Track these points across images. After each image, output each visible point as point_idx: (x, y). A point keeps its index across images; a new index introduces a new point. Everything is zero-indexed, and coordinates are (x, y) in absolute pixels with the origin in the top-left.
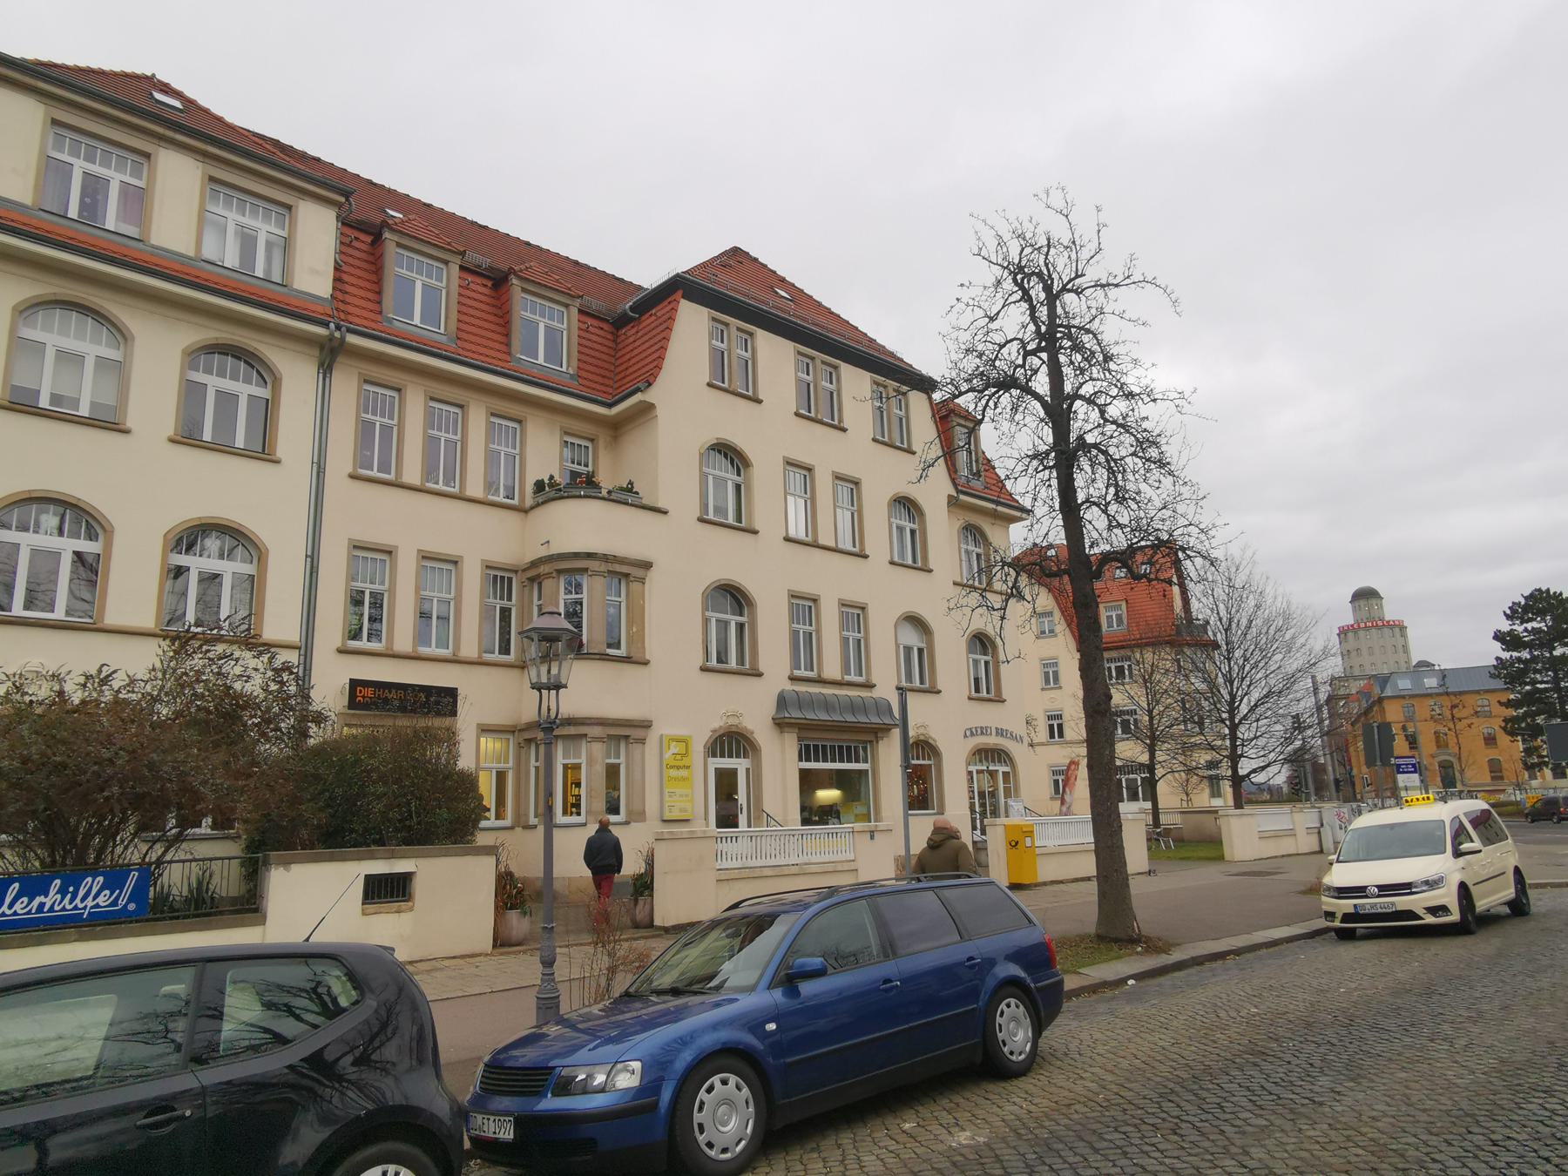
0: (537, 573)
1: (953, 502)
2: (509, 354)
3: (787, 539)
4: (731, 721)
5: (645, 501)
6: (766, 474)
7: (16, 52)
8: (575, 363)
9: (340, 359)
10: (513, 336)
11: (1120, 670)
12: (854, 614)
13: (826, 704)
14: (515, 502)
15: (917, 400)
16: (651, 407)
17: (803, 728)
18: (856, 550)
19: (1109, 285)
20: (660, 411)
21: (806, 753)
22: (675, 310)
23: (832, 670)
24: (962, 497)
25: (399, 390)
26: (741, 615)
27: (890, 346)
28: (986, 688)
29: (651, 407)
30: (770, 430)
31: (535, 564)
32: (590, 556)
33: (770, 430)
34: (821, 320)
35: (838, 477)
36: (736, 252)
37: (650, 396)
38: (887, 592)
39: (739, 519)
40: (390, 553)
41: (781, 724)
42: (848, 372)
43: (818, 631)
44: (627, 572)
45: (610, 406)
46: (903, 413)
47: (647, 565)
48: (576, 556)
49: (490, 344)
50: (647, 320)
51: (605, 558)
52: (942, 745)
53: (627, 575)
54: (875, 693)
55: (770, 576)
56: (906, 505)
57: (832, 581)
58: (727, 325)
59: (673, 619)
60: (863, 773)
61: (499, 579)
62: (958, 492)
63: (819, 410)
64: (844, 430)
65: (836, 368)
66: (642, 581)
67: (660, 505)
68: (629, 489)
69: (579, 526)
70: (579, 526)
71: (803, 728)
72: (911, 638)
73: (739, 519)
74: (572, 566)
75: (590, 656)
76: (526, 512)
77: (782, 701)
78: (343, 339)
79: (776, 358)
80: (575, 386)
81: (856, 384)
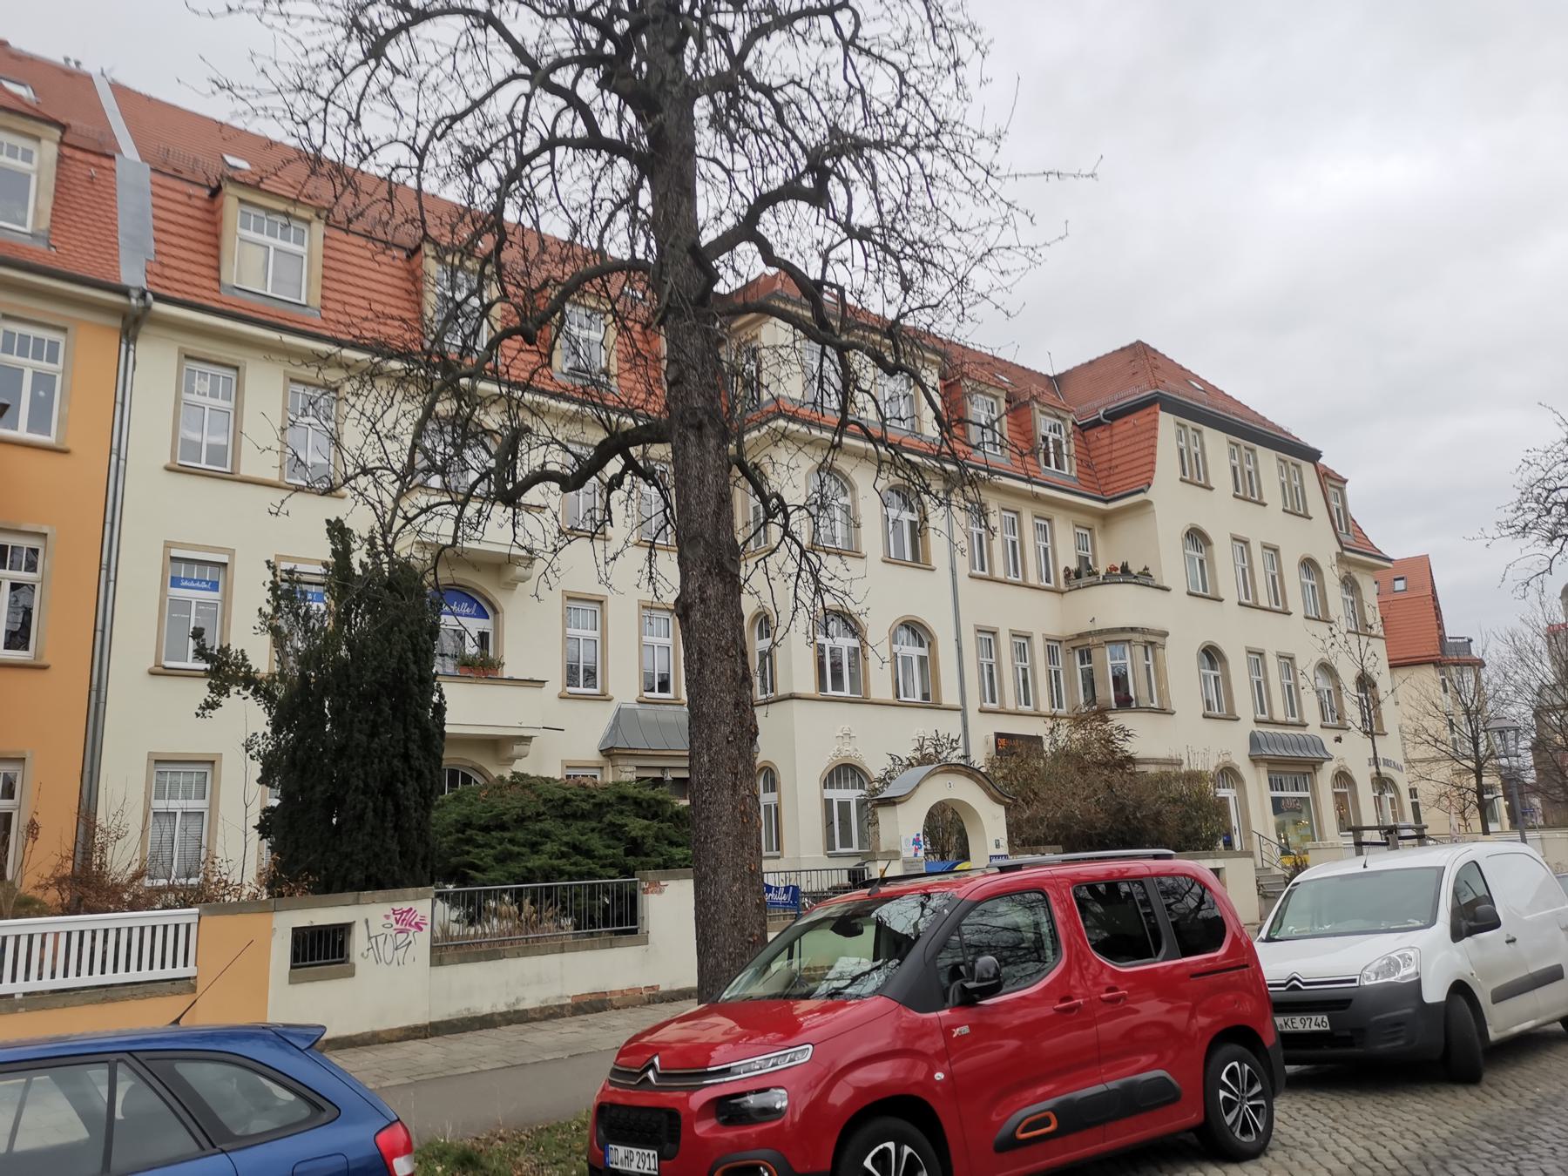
0: (1083, 646)
1: (1341, 559)
2: (218, 280)
3: (1240, 604)
4: (1227, 758)
5: (1157, 582)
6: (1223, 552)
7: (19, 42)
8: (1075, 467)
9: (145, 329)
10: (225, 257)
11: (664, 686)
12: (1288, 661)
13: (1283, 742)
14: (1052, 585)
15: (1307, 468)
16: (1148, 503)
17: (1272, 762)
18: (1280, 608)
19: (880, 58)
20: (1156, 506)
21: (1275, 784)
22: (1156, 420)
23: (1279, 715)
24: (1347, 554)
25: (237, 368)
26: (1213, 669)
27: (1278, 422)
28: (1372, 728)
29: (1147, 504)
30: (1221, 514)
31: (1080, 636)
32: (1133, 630)
33: (1221, 514)
34: (1233, 408)
35: (1265, 547)
36: (1139, 342)
37: (1150, 495)
38: (1301, 640)
39: (1205, 590)
40: (1028, 638)
41: (1255, 760)
42: (1261, 450)
43: (1266, 680)
44: (1153, 641)
45: (1106, 502)
46: (1197, 449)
47: (1165, 634)
48: (1123, 630)
49: (194, 268)
50: (1122, 427)
51: (1143, 631)
52: (1355, 775)
53: (1152, 643)
54: (1309, 731)
55: (1236, 632)
56: (1309, 565)
57: (1274, 635)
58: (1184, 426)
59: (1183, 678)
60: (1305, 800)
61: (1053, 646)
62: (1343, 549)
63: (1247, 491)
64: (1211, 489)
65: (1252, 450)
66: (1163, 647)
67: (1165, 584)
68: (1146, 573)
69: (1116, 607)
70: (1116, 607)
71: (1272, 762)
72: (1324, 684)
73: (1205, 590)
74: (1119, 636)
75: (1139, 709)
76: (1062, 593)
77: (1254, 741)
78: (148, 308)
79: (1216, 443)
80: (1074, 485)
81: (1267, 459)
